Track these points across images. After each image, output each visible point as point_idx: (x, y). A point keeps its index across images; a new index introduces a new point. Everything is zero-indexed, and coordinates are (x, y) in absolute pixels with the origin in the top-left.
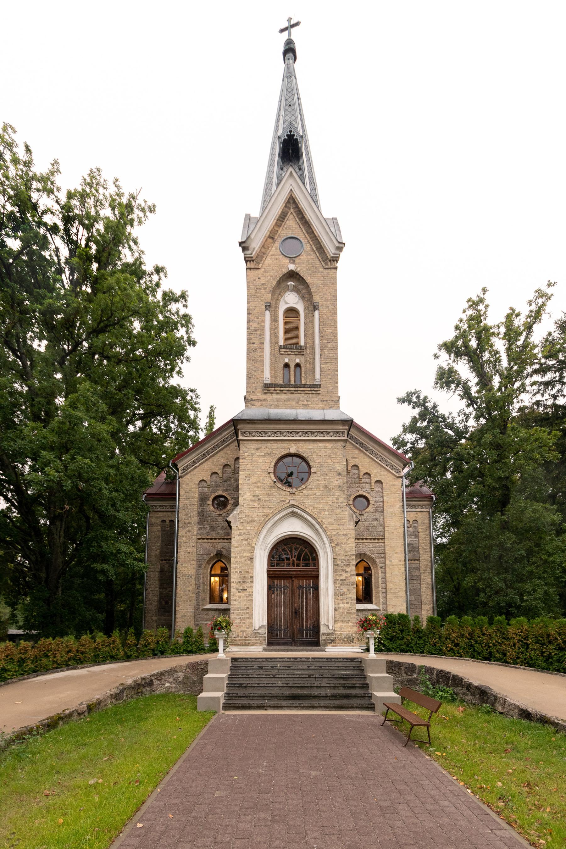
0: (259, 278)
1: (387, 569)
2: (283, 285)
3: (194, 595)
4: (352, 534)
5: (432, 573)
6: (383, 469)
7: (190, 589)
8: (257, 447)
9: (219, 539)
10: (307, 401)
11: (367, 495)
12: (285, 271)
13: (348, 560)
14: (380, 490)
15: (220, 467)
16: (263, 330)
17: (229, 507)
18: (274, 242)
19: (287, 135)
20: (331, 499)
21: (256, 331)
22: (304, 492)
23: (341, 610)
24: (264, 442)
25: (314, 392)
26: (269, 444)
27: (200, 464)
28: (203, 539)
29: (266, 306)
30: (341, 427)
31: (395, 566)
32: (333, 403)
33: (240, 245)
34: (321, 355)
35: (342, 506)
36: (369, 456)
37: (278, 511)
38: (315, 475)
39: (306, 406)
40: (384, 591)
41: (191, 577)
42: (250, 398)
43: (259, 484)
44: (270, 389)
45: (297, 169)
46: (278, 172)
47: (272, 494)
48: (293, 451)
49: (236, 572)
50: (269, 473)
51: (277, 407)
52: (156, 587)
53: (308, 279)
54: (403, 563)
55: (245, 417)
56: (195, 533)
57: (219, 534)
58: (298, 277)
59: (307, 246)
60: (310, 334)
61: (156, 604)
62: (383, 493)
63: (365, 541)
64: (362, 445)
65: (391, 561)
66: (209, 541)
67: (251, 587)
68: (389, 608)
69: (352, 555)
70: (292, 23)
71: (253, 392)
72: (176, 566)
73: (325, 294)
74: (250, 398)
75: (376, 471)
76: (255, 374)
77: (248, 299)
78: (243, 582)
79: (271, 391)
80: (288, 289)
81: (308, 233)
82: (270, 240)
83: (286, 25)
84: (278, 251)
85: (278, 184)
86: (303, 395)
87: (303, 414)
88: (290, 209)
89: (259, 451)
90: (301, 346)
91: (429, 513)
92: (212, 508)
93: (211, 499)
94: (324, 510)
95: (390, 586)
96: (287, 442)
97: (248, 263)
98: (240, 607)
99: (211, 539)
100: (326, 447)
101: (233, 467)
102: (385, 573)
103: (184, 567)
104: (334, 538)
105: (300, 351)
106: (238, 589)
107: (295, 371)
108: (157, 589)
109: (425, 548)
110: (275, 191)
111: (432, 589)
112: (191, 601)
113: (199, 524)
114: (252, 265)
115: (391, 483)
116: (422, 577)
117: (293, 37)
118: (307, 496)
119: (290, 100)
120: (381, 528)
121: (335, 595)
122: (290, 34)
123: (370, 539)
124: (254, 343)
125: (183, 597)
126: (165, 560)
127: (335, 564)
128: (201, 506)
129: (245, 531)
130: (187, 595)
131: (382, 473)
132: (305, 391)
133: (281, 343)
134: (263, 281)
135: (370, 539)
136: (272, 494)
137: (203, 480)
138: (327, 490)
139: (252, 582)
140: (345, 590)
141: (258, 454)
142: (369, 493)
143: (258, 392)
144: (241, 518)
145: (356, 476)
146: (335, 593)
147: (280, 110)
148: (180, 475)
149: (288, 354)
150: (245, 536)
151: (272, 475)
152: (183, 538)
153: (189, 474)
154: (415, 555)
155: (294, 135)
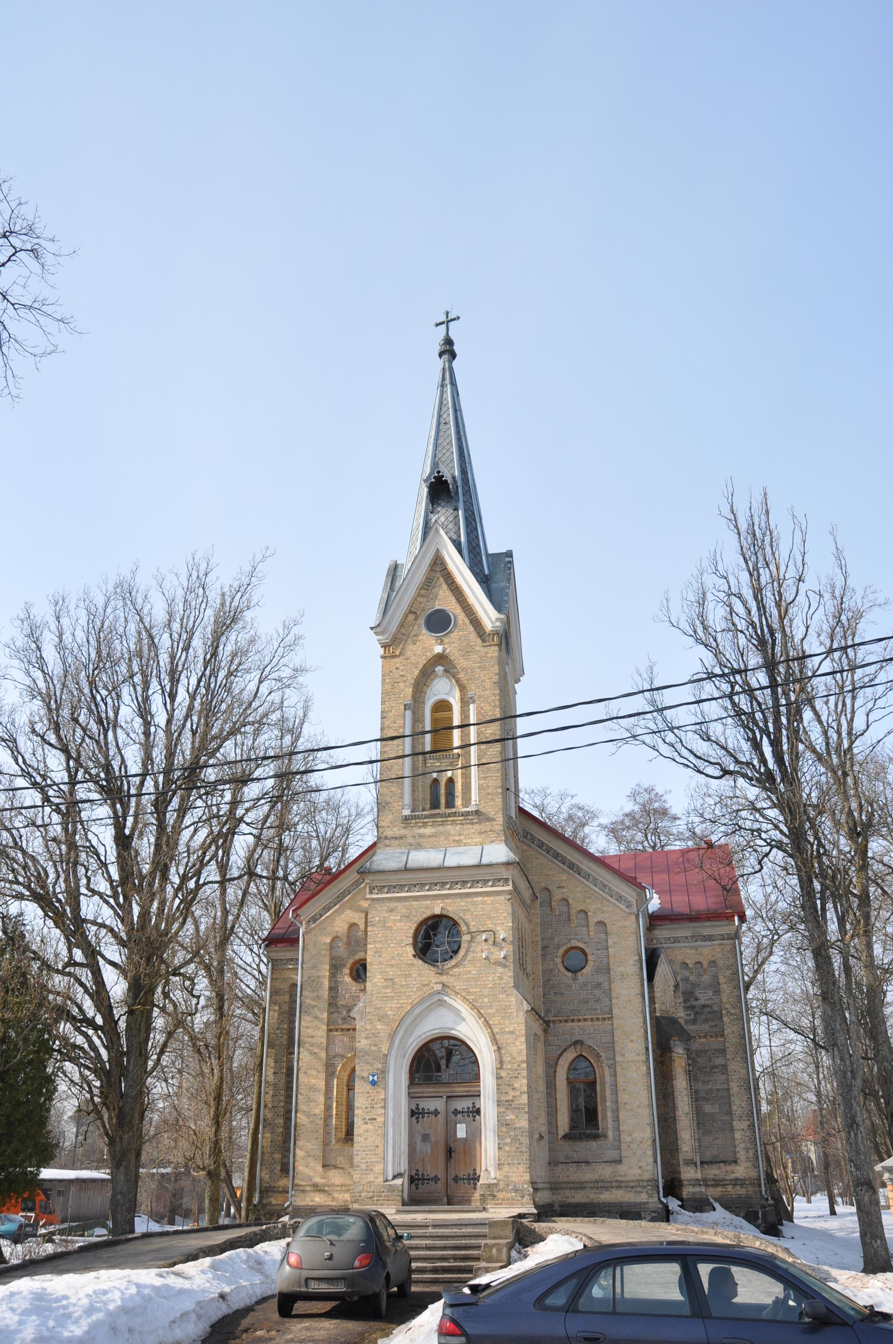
0: (397, 668)
1: (618, 1069)
6: (606, 903)
12: (429, 655)
13: (516, 1070)
14: (603, 936)
18: (416, 619)
19: (435, 478)
29: (405, 706)
43: (393, 962)
47: (409, 975)
49: (362, 1093)
52: (280, 1101)
54: (643, 1058)
59: (462, 618)
61: (281, 1130)
63: (582, 1024)
69: (522, 1062)
73: (484, 681)
75: (595, 907)
77: (382, 698)
82: (411, 617)
83: (444, 319)
89: (394, 913)
95: (623, 1097)
98: (367, 1147)
100: (484, 903)
102: (615, 1075)
108: (282, 1104)
112: (317, 1131)
115: (620, 924)
123: (592, 1020)
127: (499, 1077)
131: (605, 908)
139: (384, 1107)
141: (392, 918)
155: (443, 476)
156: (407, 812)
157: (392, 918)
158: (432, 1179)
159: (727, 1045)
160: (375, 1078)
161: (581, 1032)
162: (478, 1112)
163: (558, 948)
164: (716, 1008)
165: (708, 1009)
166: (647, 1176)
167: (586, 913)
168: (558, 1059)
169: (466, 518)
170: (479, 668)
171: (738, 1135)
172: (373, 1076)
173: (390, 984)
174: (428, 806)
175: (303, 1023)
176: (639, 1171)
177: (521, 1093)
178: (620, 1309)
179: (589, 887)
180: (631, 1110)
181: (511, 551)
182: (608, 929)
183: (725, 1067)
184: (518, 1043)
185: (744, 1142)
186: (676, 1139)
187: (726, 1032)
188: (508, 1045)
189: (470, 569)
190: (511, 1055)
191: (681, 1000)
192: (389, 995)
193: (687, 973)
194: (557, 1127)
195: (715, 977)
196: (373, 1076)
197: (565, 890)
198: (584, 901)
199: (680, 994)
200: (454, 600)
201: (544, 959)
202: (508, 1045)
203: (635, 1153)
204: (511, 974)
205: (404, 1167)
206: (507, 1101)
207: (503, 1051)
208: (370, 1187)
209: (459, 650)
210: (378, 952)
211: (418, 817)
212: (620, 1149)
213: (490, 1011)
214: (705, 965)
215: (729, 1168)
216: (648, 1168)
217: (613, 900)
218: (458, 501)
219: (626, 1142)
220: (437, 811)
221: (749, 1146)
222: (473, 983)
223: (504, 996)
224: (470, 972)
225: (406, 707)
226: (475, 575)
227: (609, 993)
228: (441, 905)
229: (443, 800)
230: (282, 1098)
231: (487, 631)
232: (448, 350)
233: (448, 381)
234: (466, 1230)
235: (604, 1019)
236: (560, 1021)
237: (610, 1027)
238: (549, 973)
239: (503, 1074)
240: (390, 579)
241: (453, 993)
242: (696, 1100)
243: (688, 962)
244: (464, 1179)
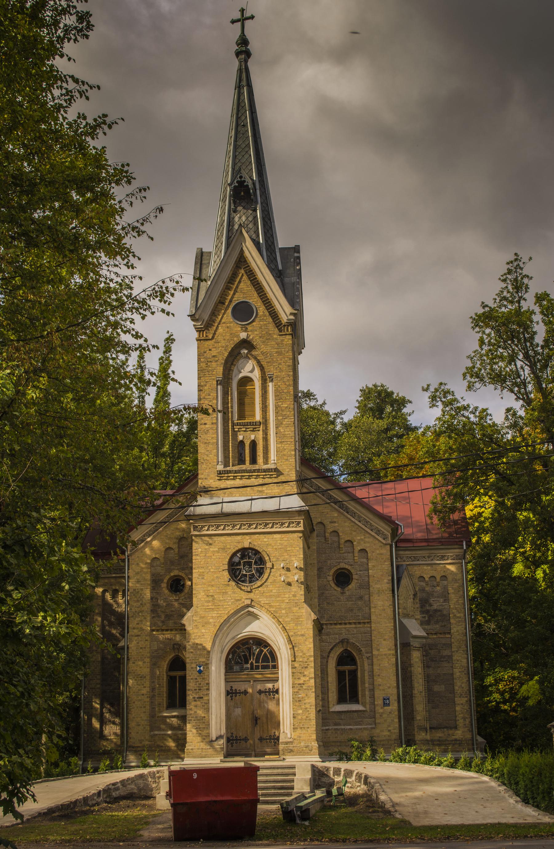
0: (210, 350)
1: (375, 660)
3: (148, 699)
6: (367, 535)
12: (236, 340)
14: (365, 560)
15: (175, 540)
20: (287, 596)
23: (300, 717)
26: (223, 538)
29: (217, 381)
40: (372, 688)
43: (213, 583)
54: (393, 652)
59: (262, 310)
62: (368, 564)
63: (348, 626)
65: (378, 650)
67: (208, 695)
69: (310, 656)
71: (206, 479)
73: (280, 364)
75: (359, 538)
76: (208, 458)
83: (238, 16)
91: (462, 566)
95: (378, 681)
100: (281, 539)
102: (372, 665)
105: (255, 426)
108: (99, 686)
109: (458, 615)
111: (469, 674)
112: (145, 707)
113: (152, 611)
115: (378, 552)
116: (454, 658)
120: (367, 608)
123: (355, 623)
124: (205, 424)
125: (136, 703)
129: (199, 634)
130: (140, 700)
131: (367, 540)
134: (214, 353)
135: (355, 623)
139: (208, 689)
141: (211, 549)
142: (351, 565)
143: (211, 478)
154: (445, 626)
155: (245, 181)
156: (220, 467)
158: (243, 740)
159: (453, 640)
160: (202, 668)
161: (347, 632)
162: (277, 692)
163: (330, 569)
164: (445, 613)
165: (439, 613)
168: (330, 652)
169: (263, 219)
170: (276, 352)
171: (458, 708)
172: (200, 667)
173: (211, 599)
174: (237, 462)
175: (130, 626)
176: (388, 733)
177: (310, 678)
179: (354, 523)
181: (299, 246)
182: (369, 555)
183: (450, 657)
184: (307, 643)
185: (462, 713)
186: (413, 711)
187: (452, 631)
188: (300, 644)
189: (267, 266)
190: (302, 651)
191: (418, 605)
193: (423, 584)
194: (328, 702)
195: (445, 588)
196: (200, 667)
197: (337, 524)
198: (351, 534)
199: (418, 601)
200: (256, 294)
201: (319, 577)
202: (300, 644)
203: (385, 721)
204: (303, 593)
205: (223, 731)
207: (296, 649)
209: (260, 337)
210: (202, 575)
211: (230, 472)
212: (375, 718)
213: (287, 620)
214: (438, 579)
215: (451, 732)
216: (395, 731)
217: (373, 534)
218: (256, 203)
220: (243, 467)
221: (466, 716)
222: (274, 599)
223: (297, 609)
225: (218, 383)
226: (272, 270)
227: (368, 604)
228: (249, 541)
229: (248, 459)
230: (99, 681)
231: (283, 322)
233: (244, 83)
235: (364, 623)
236: (331, 624)
237: (369, 629)
238: (322, 589)
239: (296, 665)
240: (198, 266)
241: (259, 606)
242: (428, 682)
243: (425, 576)
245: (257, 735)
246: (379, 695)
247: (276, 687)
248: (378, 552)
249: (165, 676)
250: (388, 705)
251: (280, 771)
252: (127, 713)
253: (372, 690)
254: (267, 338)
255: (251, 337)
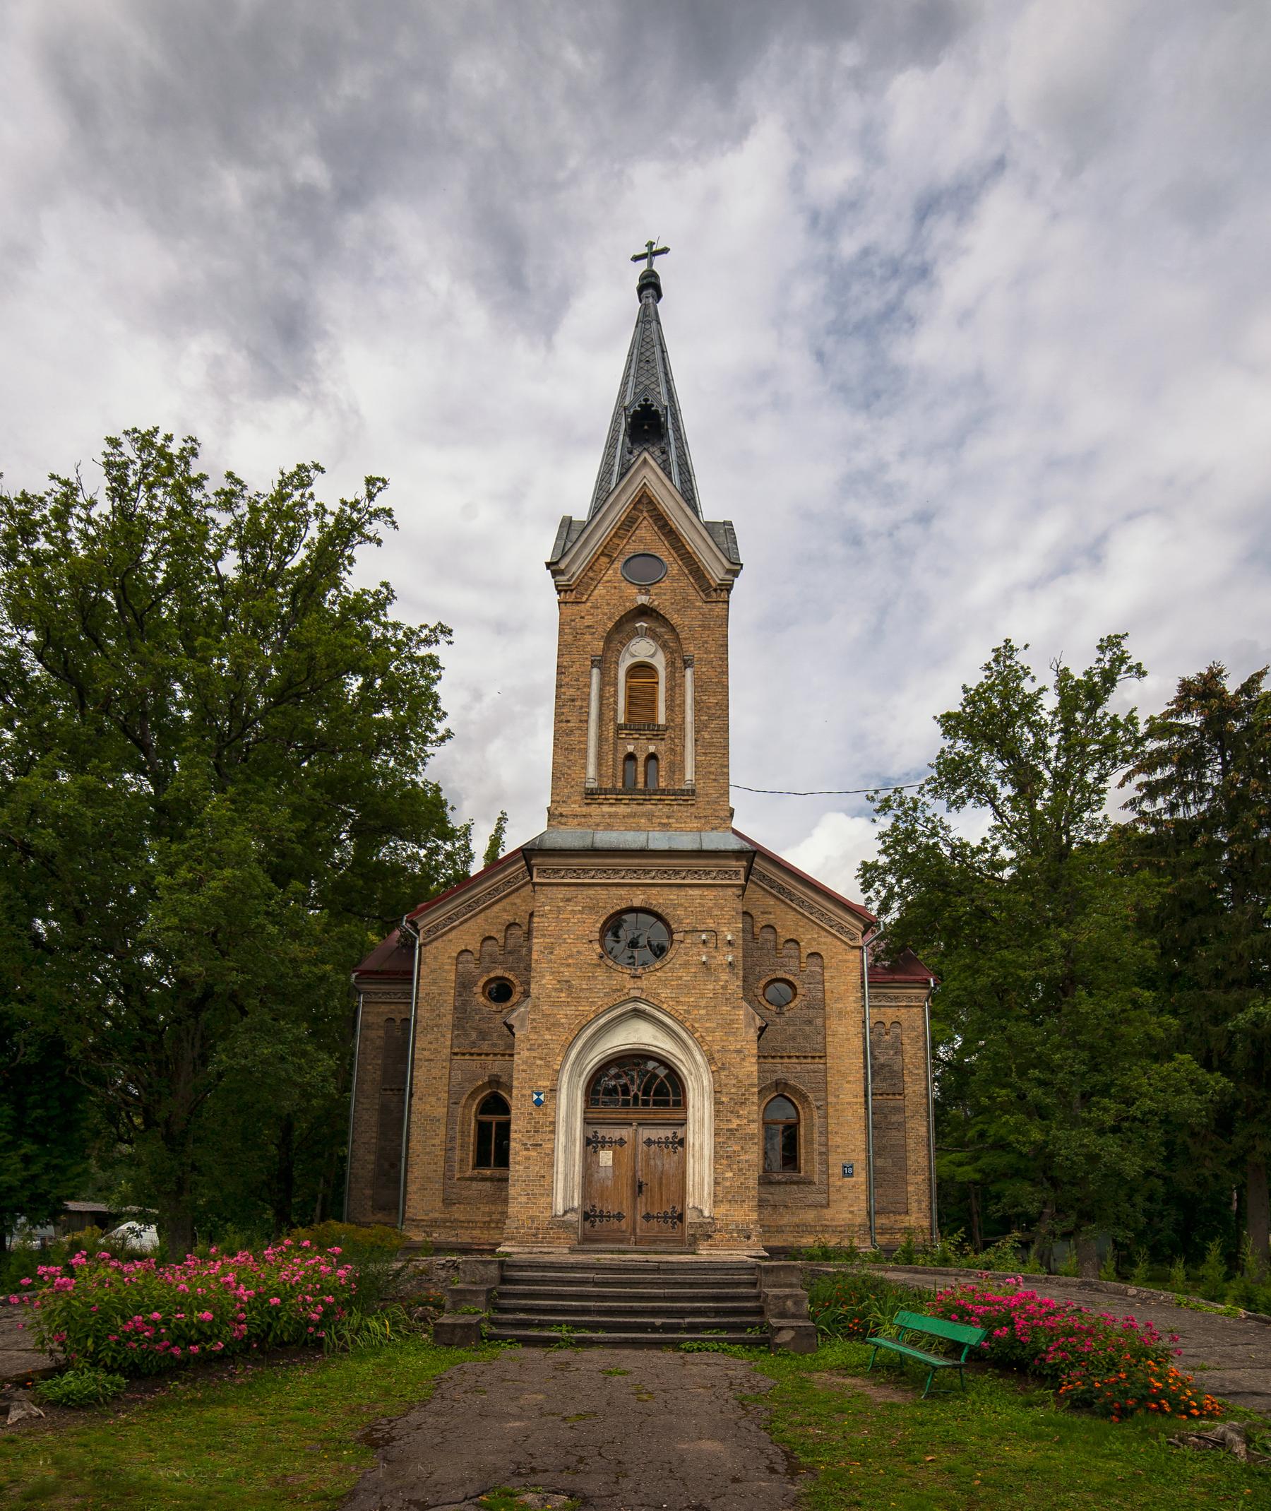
1: (831, 1110)
2: (628, 628)
3: (443, 1153)
4: (753, 1048)
5: (928, 1117)
6: (824, 933)
7: (436, 1142)
8: (570, 896)
9: (495, 1055)
10: (668, 817)
11: (791, 978)
14: (818, 969)
16: (587, 698)
17: (514, 999)
18: (612, 562)
21: (573, 700)
22: (658, 974)
24: (582, 888)
25: (681, 802)
26: (591, 892)
27: (461, 923)
28: (464, 1054)
29: (592, 662)
30: (734, 863)
31: (846, 1106)
32: (719, 821)
33: (548, 568)
34: (696, 740)
35: (732, 1000)
36: (795, 910)
37: (606, 1007)
38: (682, 945)
39: (665, 827)
41: (439, 1120)
42: (557, 813)
43: (570, 961)
44: (596, 797)
45: (658, 453)
46: (622, 456)
47: (595, 978)
48: (637, 903)
50: (591, 941)
51: (609, 827)
53: (675, 619)
54: (863, 1100)
55: (549, 844)
56: (449, 1043)
57: (494, 1045)
58: (654, 614)
59: (674, 566)
60: (674, 705)
62: (822, 974)
63: (786, 1060)
64: (782, 890)
66: (475, 1057)
68: (831, 1180)
69: (752, 1085)
70: (654, 249)
71: (564, 802)
72: (410, 1101)
73: (706, 642)
74: (557, 813)
78: (535, 1132)
79: (599, 801)
80: (636, 633)
81: (674, 549)
82: (604, 560)
83: (646, 250)
84: (619, 575)
85: (622, 476)
86: (661, 807)
87: (659, 841)
88: (642, 511)
89: (570, 903)
90: (659, 726)
92: (482, 999)
93: (481, 984)
94: (697, 1007)
95: (835, 1140)
96: (628, 888)
97: (562, 594)
99: (480, 1054)
100: (702, 897)
101: (525, 928)
102: (826, 1117)
103: (425, 1103)
104: (716, 1056)
105: (657, 732)
106: (526, 1144)
107: (646, 766)
108: (374, 1141)
110: (617, 485)
111: (929, 1145)
114: (571, 597)
115: (840, 957)
116: (907, 1126)
117: (654, 268)
118: (664, 983)
119: (648, 354)
121: (717, 1157)
122: (650, 264)
123: (798, 1057)
124: (568, 721)
126: (392, 1090)
127: (717, 1102)
128: (460, 996)
129: (540, 1042)
131: (823, 940)
132: (664, 800)
133: (621, 719)
134: (588, 622)
135: (798, 1057)
136: (595, 978)
137: (466, 951)
138: (703, 972)
139: (553, 1132)
140: (736, 1148)
141: (570, 908)
142: (795, 975)
143: (575, 802)
144: (534, 1020)
145: (771, 944)
146: (716, 1152)
147: (630, 368)
148: (422, 941)
149: (634, 739)
150: (540, 1050)
151: (597, 946)
152: (425, 1053)
153: (440, 940)
157: (570, 908)
158: (614, 1216)
160: (542, 1097)
162: (682, 1142)
163: (760, 979)
166: (858, 1221)
167: (798, 943)
170: (700, 626)
171: (911, 1189)
172: (539, 1094)
175: (417, 1045)
178: (596, 845)
179: (803, 915)
180: (844, 1154)
184: (746, 1064)
187: (906, 1092)
192: (563, 999)
195: (897, 1036)
196: (539, 1094)
205: (576, 1203)
206: (728, 1130)
208: (533, 1222)
214: (888, 1025)
215: (898, 1217)
219: (835, 1186)
224: (681, 978)
227: (823, 1032)
232: (650, 286)
234: (712, 1277)
244: (658, 1217)
245: (642, 1210)
246: (836, 1160)
247: (680, 1135)
248: (840, 957)
249: (473, 1122)
250: (851, 1175)
251: (718, 1277)
252: (406, 1171)
253: (825, 1154)
254: (684, 605)
255: (656, 603)
